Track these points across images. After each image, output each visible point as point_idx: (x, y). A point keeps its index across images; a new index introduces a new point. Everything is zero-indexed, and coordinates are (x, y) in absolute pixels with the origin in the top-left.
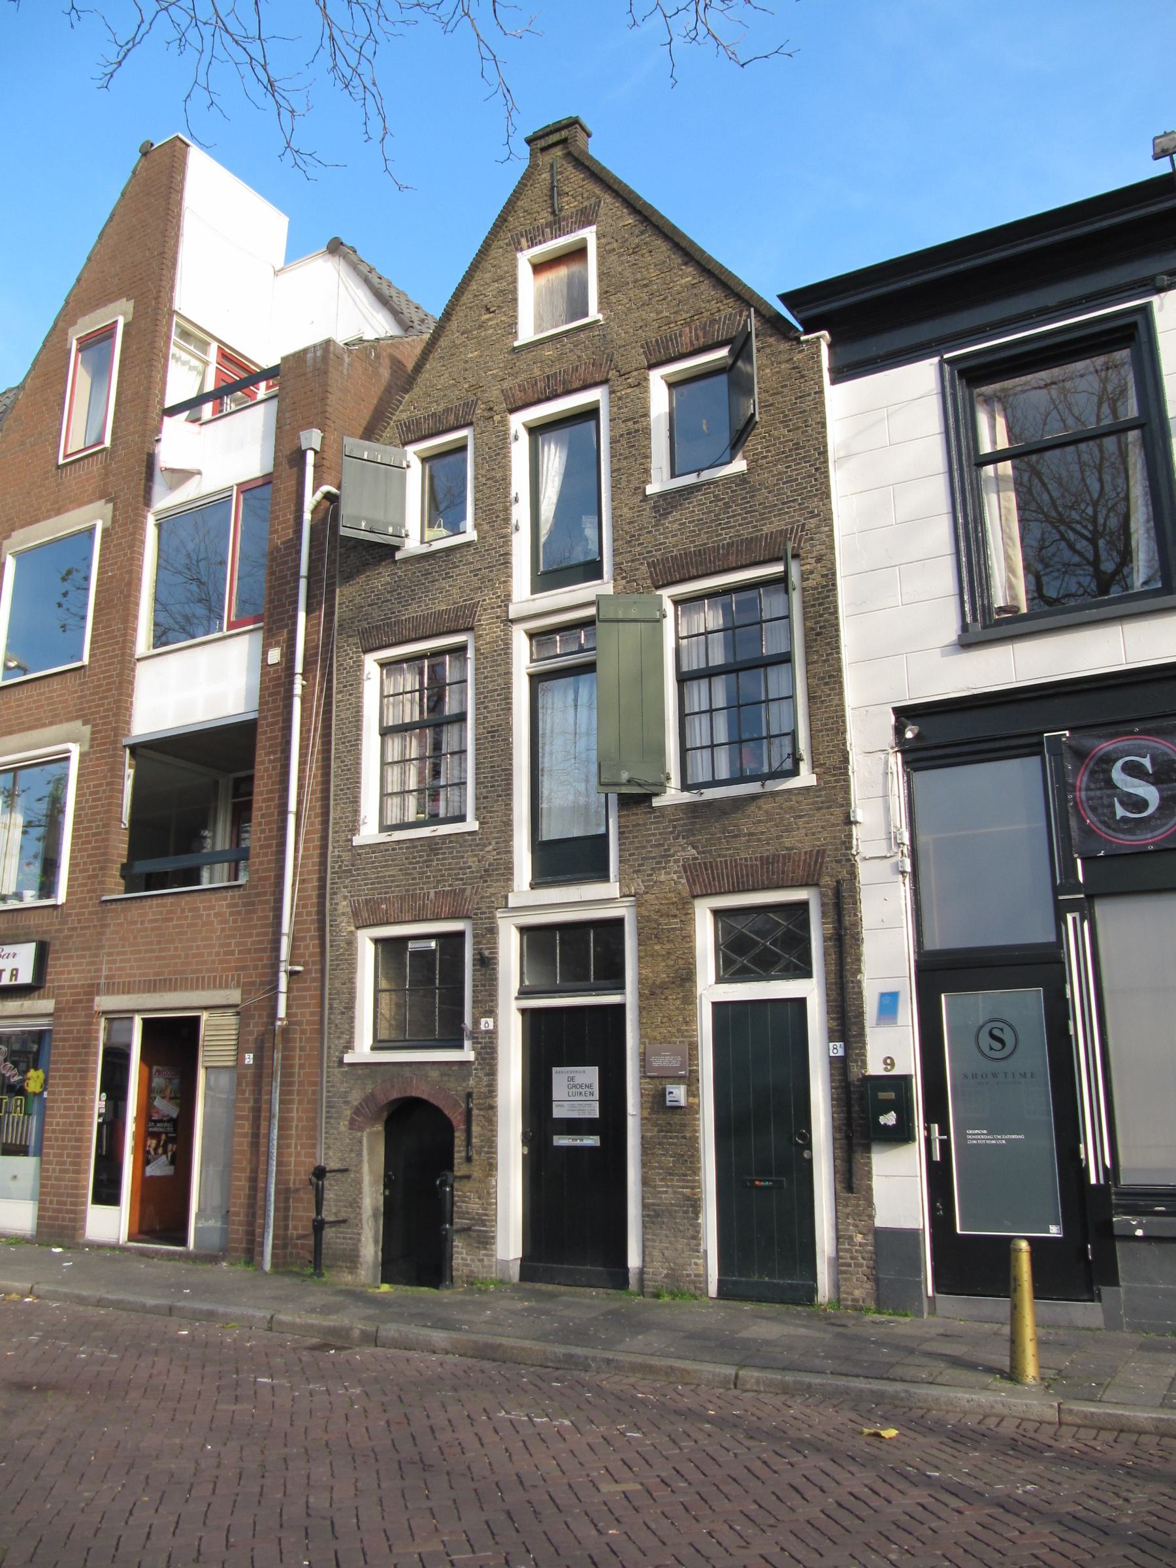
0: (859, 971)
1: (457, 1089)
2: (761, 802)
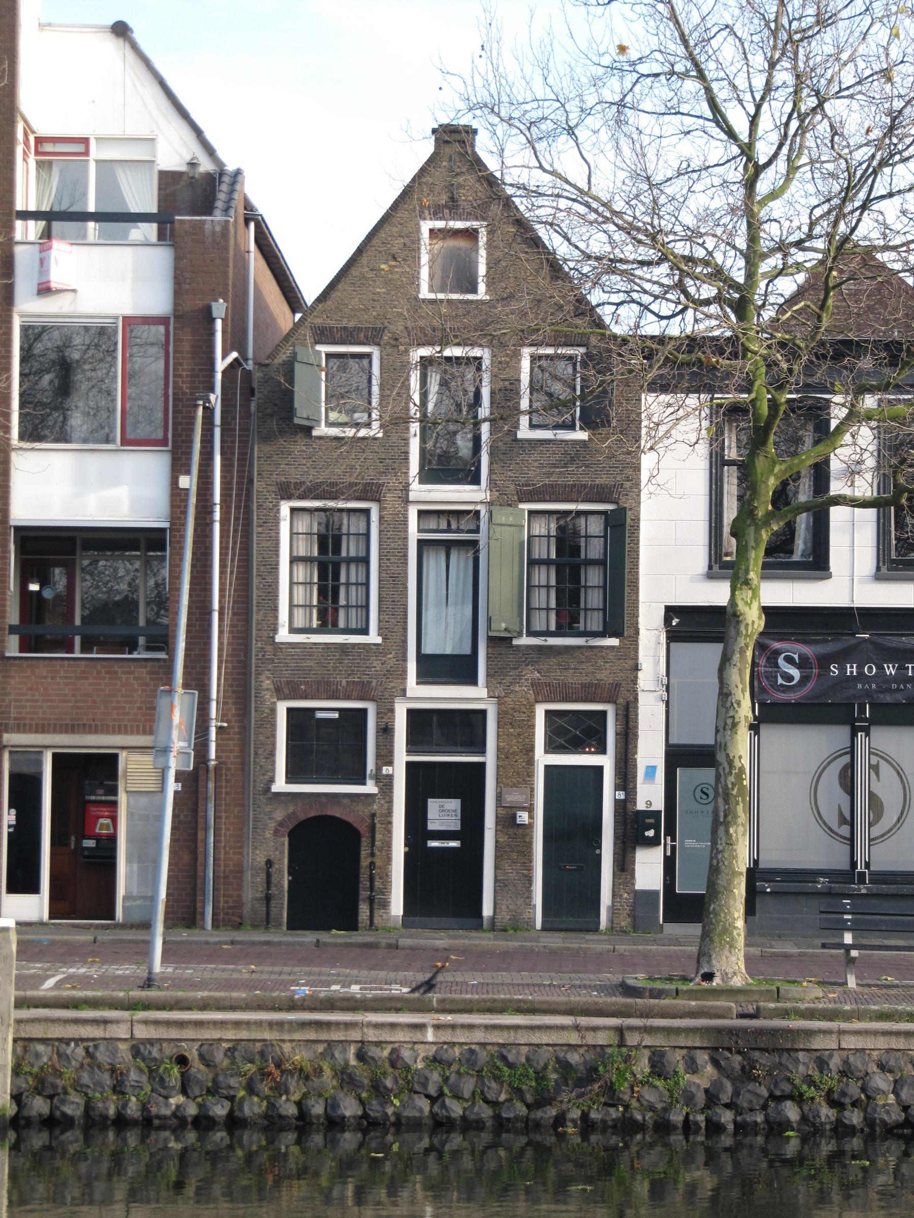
0: (636, 753)
1: (363, 811)
2: (584, 650)
